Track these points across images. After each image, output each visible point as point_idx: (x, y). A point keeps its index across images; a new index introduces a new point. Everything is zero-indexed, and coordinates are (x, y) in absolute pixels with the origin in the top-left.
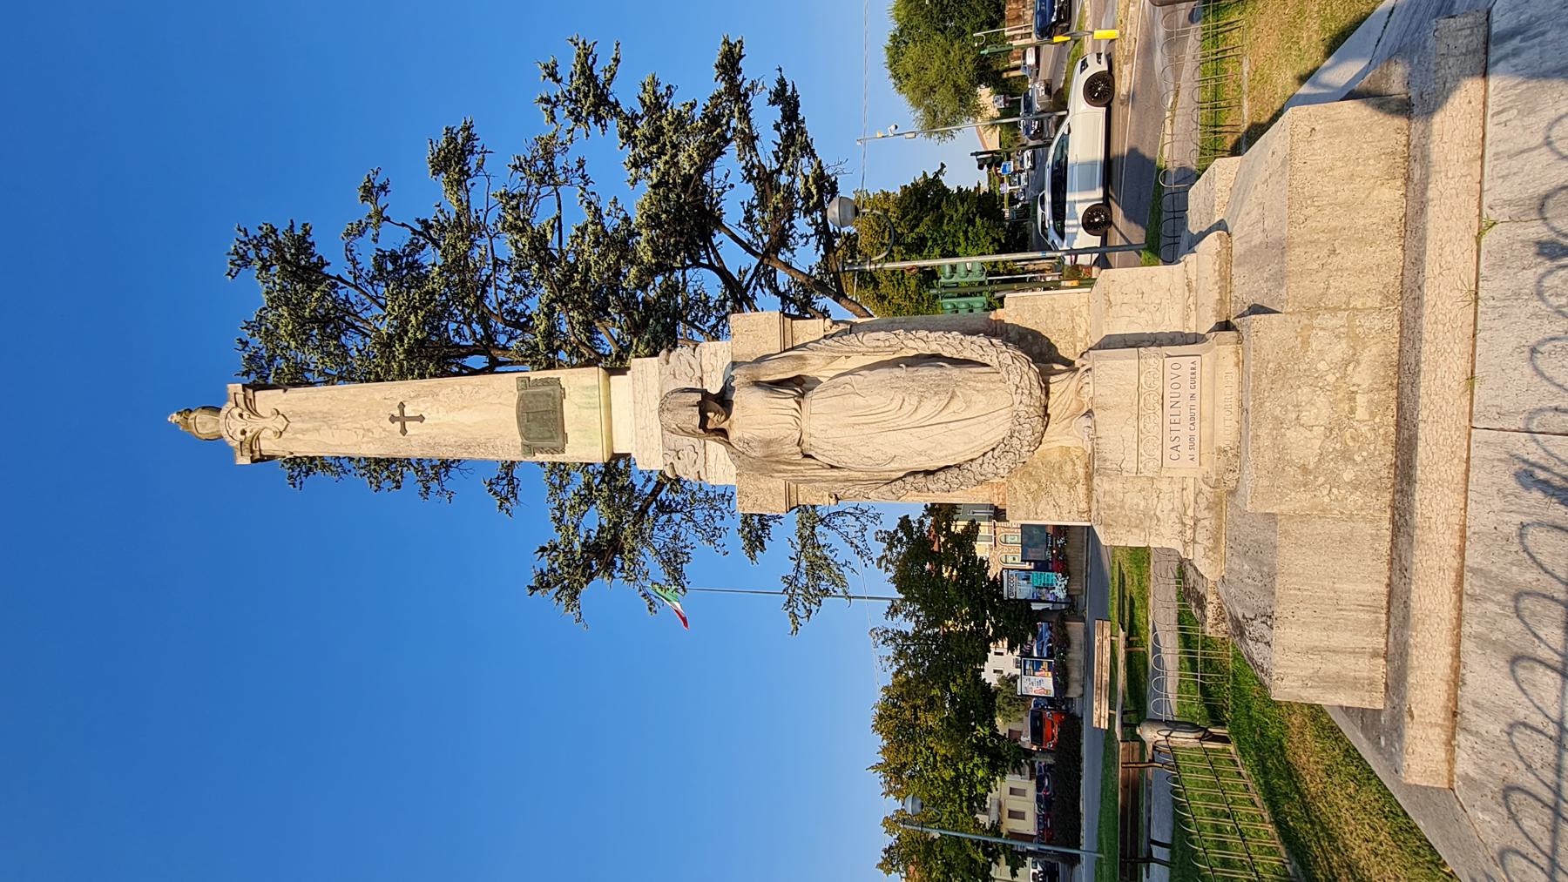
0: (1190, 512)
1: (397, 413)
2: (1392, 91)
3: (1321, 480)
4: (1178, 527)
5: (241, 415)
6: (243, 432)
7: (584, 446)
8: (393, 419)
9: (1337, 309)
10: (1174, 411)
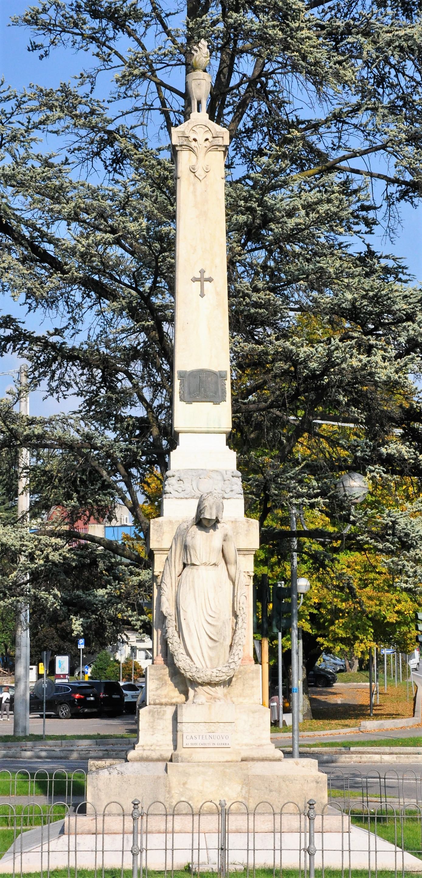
0: (157, 748)
1: (206, 276)
2: (23, 413)
3: (181, 790)
4: (149, 743)
5: (207, 140)
6: (195, 140)
7: (186, 415)
8: (202, 272)
9: (249, 793)
10: (208, 737)
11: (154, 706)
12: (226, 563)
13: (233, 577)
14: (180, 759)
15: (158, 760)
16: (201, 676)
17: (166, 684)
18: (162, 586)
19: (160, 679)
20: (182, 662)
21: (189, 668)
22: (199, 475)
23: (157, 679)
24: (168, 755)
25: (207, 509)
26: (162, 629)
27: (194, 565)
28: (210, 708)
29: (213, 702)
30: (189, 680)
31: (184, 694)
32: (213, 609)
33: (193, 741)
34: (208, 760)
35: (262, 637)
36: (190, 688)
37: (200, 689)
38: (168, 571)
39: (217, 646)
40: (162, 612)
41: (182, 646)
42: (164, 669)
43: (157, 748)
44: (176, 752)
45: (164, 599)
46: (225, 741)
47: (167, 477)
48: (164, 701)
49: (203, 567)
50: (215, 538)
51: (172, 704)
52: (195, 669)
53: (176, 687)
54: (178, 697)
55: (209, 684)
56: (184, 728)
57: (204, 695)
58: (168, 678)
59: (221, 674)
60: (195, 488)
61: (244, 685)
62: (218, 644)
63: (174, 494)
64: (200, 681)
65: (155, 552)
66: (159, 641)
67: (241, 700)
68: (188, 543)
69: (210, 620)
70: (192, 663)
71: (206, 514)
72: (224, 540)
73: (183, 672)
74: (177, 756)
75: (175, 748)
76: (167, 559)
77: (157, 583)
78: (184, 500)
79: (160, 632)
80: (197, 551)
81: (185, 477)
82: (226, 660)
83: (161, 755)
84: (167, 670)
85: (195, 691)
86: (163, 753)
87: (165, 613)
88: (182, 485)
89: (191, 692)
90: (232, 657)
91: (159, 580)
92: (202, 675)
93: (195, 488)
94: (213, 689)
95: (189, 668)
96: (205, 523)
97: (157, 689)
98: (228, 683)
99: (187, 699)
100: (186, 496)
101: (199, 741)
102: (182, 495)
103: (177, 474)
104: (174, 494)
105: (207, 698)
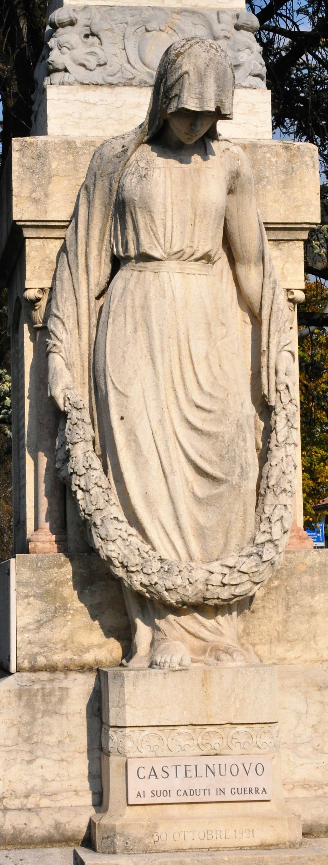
0: (45, 802)
4: (20, 788)
10: (202, 770)
11: (33, 676)
12: (233, 261)
13: (255, 299)
14: (119, 842)
15: (49, 841)
16: (180, 585)
17: (66, 609)
18: (51, 326)
19: (48, 595)
20: (116, 543)
21: (138, 560)
22: (146, 22)
23: (41, 597)
24: (79, 825)
25: (191, 81)
26: (51, 453)
27: (146, 258)
28: (205, 681)
29: (212, 660)
30: (139, 596)
31: (118, 639)
32: (207, 388)
33: (159, 784)
34: (206, 843)
35: (79, 501)
36: (139, 622)
37: (170, 624)
38: (67, 285)
39: (220, 496)
40: (52, 400)
41: (114, 498)
42: (61, 566)
43: (45, 802)
44: (105, 820)
45: (56, 361)
46: (253, 781)
47: (55, 27)
48: (59, 658)
49: (173, 264)
50: (208, 176)
51: (83, 668)
52: (157, 565)
53: (94, 617)
54: (100, 646)
55: (203, 607)
56: (129, 744)
57: (183, 640)
58: (69, 592)
59: (236, 578)
60: (134, 58)
61: (288, 608)
62: (223, 488)
63: (76, 72)
64: (172, 598)
65: (27, 233)
66: (42, 487)
67: (280, 651)
68: (127, 195)
69: (196, 418)
70: (148, 547)
71: (185, 95)
72: (230, 191)
73: (120, 572)
74: (111, 833)
75: (100, 801)
76: (64, 249)
77: (31, 323)
78: (106, 90)
79: (43, 460)
80: (158, 218)
81: (105, 26)
82: (249, 535)
83: (57, 826)
84: (67, 570)
85: (156, 629)
86: (63, 818)
87: (60, 402)
88: (97, 50)
89: (143, 633)
90: (264, 526)
91: (39, 315)
92: (179, 581)
93: (134, 58)
94: (210, 623)
95: (138, 560)
96: (179, 129)
97: (40, 624)
98: (243, 604)
99: (129, 651)
100: (110, 80)
101: (176, 783)
102: (97, 75)
103: (82, 19)
104: (76, 72)
105: (193, 650)
